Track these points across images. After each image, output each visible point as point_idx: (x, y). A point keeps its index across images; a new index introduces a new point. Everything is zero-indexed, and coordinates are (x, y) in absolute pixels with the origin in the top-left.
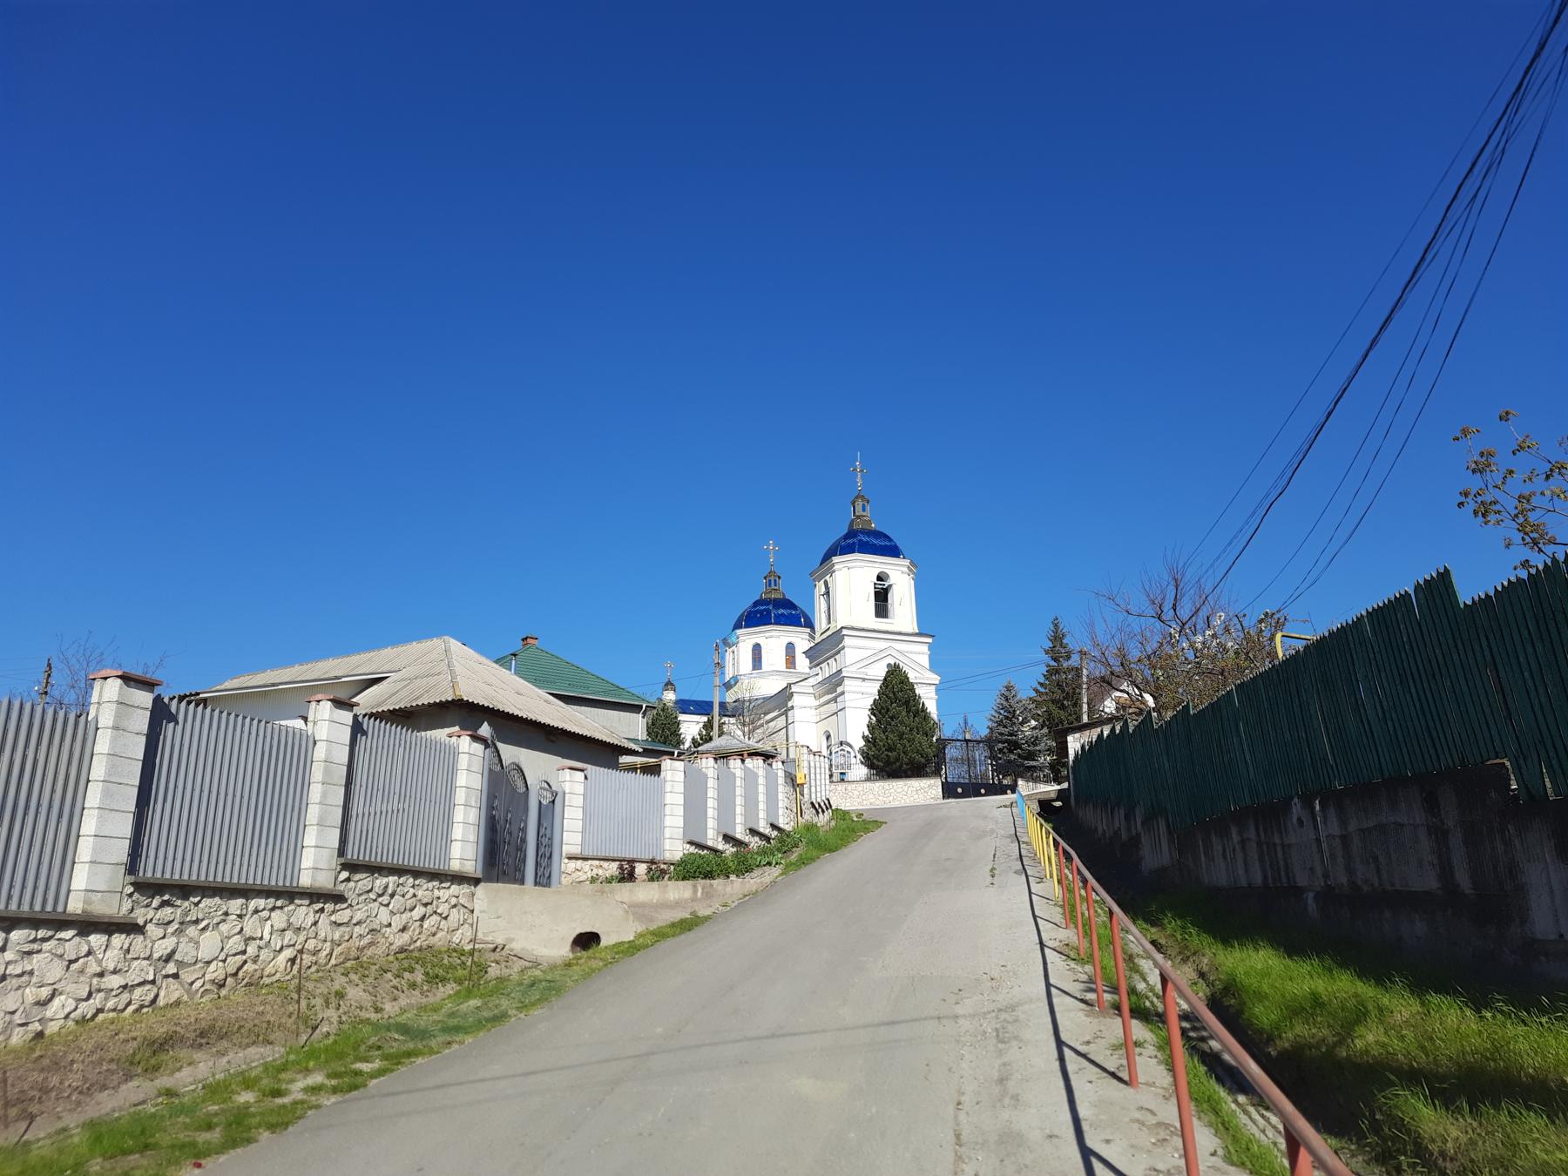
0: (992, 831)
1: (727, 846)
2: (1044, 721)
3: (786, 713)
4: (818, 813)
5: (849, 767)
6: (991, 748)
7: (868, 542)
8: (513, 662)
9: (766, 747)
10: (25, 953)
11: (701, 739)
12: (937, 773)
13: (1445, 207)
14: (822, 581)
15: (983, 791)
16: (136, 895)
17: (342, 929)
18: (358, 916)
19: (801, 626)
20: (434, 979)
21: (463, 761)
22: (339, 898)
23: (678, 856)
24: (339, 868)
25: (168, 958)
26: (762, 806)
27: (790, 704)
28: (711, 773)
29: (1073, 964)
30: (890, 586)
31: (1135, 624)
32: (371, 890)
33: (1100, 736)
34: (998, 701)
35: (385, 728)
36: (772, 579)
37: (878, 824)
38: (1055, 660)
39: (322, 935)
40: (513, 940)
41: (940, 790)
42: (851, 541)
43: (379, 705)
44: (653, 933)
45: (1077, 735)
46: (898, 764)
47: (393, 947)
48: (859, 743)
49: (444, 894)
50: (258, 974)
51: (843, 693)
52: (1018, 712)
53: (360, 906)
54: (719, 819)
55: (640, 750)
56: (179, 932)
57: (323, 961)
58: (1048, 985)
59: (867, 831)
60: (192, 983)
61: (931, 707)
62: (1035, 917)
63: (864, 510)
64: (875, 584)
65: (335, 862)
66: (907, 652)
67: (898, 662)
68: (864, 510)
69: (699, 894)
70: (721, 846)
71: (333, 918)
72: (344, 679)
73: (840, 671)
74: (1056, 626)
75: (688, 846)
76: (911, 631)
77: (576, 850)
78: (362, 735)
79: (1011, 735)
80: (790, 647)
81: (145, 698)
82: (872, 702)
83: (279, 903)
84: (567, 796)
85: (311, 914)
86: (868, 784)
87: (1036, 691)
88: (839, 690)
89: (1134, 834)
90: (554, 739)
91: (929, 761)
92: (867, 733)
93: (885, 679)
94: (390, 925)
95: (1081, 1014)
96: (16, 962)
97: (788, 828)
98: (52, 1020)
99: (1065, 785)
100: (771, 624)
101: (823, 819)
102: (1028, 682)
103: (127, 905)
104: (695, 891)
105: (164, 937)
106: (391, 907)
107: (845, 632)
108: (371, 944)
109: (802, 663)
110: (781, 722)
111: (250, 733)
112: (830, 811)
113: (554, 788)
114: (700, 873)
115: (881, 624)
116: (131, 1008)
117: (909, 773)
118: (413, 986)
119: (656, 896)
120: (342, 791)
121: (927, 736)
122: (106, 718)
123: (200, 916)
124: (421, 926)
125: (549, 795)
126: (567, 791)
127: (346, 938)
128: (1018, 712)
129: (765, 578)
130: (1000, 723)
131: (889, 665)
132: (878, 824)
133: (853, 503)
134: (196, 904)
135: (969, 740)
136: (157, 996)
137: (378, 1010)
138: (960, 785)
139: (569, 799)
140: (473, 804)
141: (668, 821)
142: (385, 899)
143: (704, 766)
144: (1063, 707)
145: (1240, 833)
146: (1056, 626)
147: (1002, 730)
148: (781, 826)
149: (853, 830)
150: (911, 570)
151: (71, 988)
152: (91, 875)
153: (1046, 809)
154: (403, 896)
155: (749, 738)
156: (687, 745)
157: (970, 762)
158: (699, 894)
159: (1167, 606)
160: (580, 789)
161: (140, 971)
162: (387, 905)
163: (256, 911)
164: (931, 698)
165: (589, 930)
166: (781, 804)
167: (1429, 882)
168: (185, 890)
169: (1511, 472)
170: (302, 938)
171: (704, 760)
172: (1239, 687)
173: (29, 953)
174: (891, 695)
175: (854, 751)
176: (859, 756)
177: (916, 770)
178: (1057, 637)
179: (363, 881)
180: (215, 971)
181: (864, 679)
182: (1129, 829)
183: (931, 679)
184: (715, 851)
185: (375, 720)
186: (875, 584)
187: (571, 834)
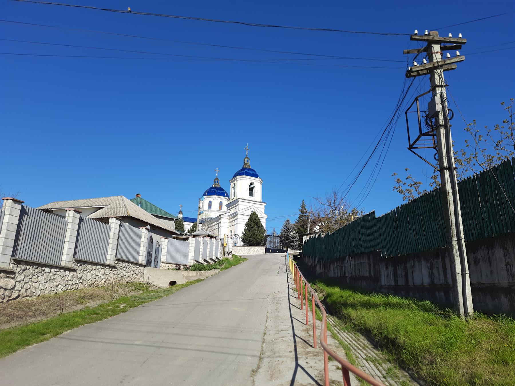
0: (279, 263)
1: (204, 263)
2: (297, 231)
3: (218, 224)
4: (229, 255)
5: (237, 242)
6: (281, 239)
7: (248, 172)
8: (140, 204)
9: (211, 234)
10: (54, 274)
11: (191, 230)
12: (264, 245)
13: (382, 135)
14: (233, 183)
15: (277, 252)
16: (75, 263)
17: (115, 275)
18: (119, 272)
19: (225, 197)
20: (138, 289)
21: (143, 235)
22: (115, 267)
23: (192, 264)
24: (115, 260)
25: (81, 278)
26: (214, 252)
27: (220, 221)
28: (202, 242)
29: (294, 292)
30: (254, 186)
31: (323, 207)
32: (122, 266)
33: (310, 238)
34: (284, 224)
35: (95, 222)
36: (217, 181)
37: (246, 259)
38: (302, 213)
39: (111, 276)
40: (154, 282)
41: (265, 250)
42: (243, 171)
43: (103, 215)
44: (190, 282)
45: (306, 237)
46: (253, 242)
47: (126, 281)
48: (241, 235)
49: (138, 269)
50: (98, 284)
51: (237, 219)
52: (290, 228)
53: (119, 270)
54: (203, 255)
55: (179, 234)
56: (83, 272)
57: (111, 283)
58: (290, 304)
59: (243, 261)
60: (85, 285)
61: (264, 225)
62: (288, 282)
63: (248, 162)
64: (250, 185)
65: (114, 259)
66: (258, 208)
67: (255, 210)
68: (248, 162)
69: (198, 275)
70: (203, 262)
71: (114, 272)
72: (93, 207)
73: (237, 212)
74: (303, 203)
75: (195, 262)
76: (259, 201)
77: (164, 261)
78: (25, 215)
79: (287, 235)
80: (221, 203)
81: (19, 207)
82: (246, 222)
83: (103, 268)
84: (163, 246)
85: (109, 271)
86: (243, 248)
87: (296, 222)
88: (236, 218)
89: (315, 264)
90: (154, 229)
91: (262, 241)
92: (244, 232)
93: (251, 216)
94: (125, 276)
95: (294, 300)
96: (52, 276)
97: (221, 259)
98: (58, 290)
99: (301, 251)
100: (215, 195)
101: (230, 257)
102: (293, 220)
103: (73, 265)
104: (197, 274)
105: (80, 273)
106: (126, 271)
107: (239, 200)
108: (121, 280)
109: (225, 208)
110: (217, 226)
111: (49, 218)
112: (232, 255)
113: (159, 243)
114: (198, 269)
115: (251, 198)
116: (73, 289)
117: (256, 245)
118: (133, 290)
119: (186, 275)
120: (117, 241)
121: (262, 234)
122: (70, 220)
123: (87, 269)
124: (132, 276)
125: (158, 245)
126: (163, 244)
127: (116, 278)
128: (290, 228)
129: (214, 180)
130: (284, 231)
131: (252, 211)
132: (246, 259)
133: (245, 159)
134: (86, 266)
135: (275, 236)
136: (78, 287)
137: (126, 295)
138: (270, 249)
139: (164, 247)
140: (145, 246)
141: (190, 254)
142: (125, 269)
143: (200, 239)
144: (303, 228)
145: (337, 264)
146: (303, 203)
147: (285, 233)
148: (219, 258)
149: (239, 260)
150: (261, 182)
151: (62, 283)
152: (67, 257)
153: (295, 258)
154: (129, 268)
155: (207, 231)
156: (186, 232)
157: (274, 243)
158: (198, 275)
159: (332, 203)
160: (166, 244)
161: (75, 281)
162: (125, 270)
163: (98, 269)
164: (265, 222)
165: (174, 280)
166: (219, 252)
167: (367, 274)
168: (85, 262)
169: (405, 184)
170: (107, 277)
171: (200, 238)
172: (339, 229)
173: (55, 274)
174: (252, 221)
175: (239, 237)
176: (241, 239)
177: (258, 244)
178: (303, 207)
179: (120, 264)
180: (90, 282)
181: (244, 215)
182: (314, 263)
183: (265, 216)
184: (202, 264)
185: (43, 212)
186: (250, 185)
187: (163, 256)
